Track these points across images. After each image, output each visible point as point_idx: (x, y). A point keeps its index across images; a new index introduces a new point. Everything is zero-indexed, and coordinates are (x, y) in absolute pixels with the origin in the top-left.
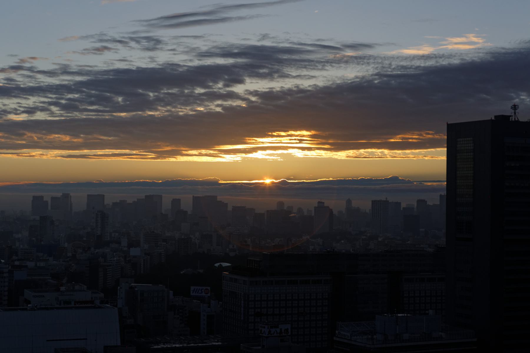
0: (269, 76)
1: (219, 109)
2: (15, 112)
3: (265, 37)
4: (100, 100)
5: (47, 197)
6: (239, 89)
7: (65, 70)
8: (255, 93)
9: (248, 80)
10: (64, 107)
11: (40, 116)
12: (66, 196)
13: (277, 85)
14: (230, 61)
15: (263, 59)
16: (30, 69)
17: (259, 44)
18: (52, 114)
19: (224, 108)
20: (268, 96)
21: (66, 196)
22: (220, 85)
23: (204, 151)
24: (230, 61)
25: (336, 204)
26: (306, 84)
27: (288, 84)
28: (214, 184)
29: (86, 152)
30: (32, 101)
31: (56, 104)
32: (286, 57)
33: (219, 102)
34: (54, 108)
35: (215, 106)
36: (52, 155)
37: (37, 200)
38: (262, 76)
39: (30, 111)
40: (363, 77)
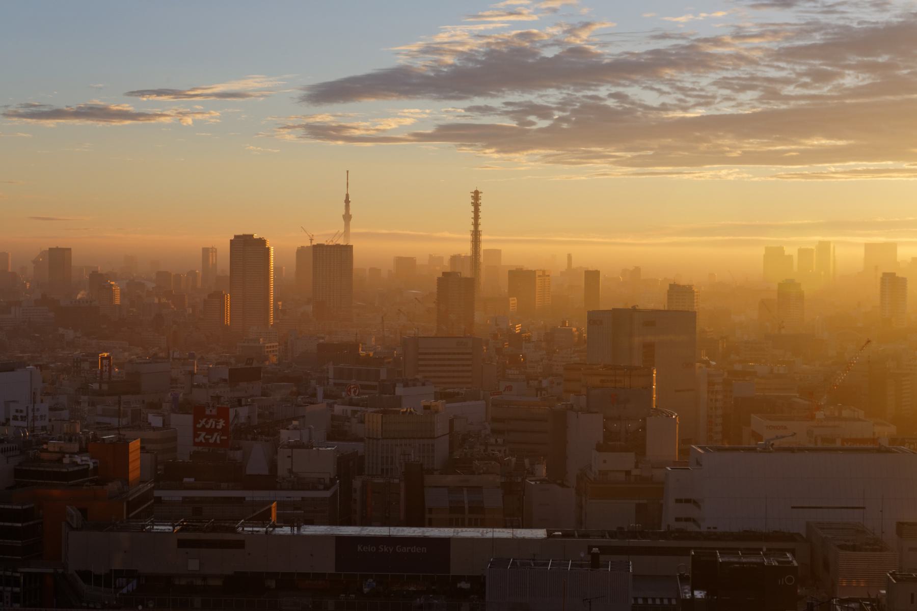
11: (726, 109)
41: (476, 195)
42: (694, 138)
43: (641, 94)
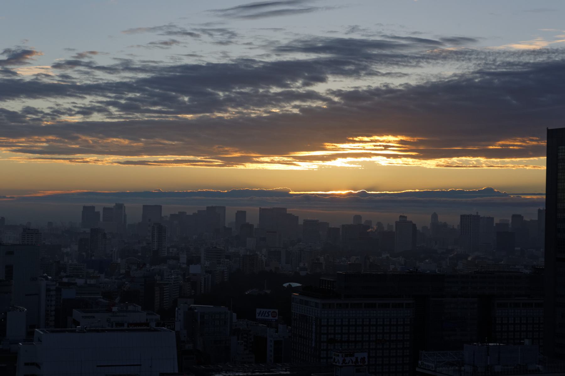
0: (355, 73)
1: (296, 111)
2: (69, 112)
3: (353, 29)
4: (164, 100)
5: (99, 207)
6: (320, 88)
7: (127, 66)
8: (339, 93)
9: (331, 78)
10: (123, 108)
11: (97, 117)
12: (120, 207)
13: (364, 83)
14: (312, 56)
15: (349, 54)
16: (88, 65)
17: (347, 37)
18: (110, 115)
19: (303, 110)
20: (353, 96)
21: (120, 207)
22: (299, 83)
23: (277, 158)
24: (312, 56)
25: (421, 219)
26: (396, 83)
27: (375, 82)
28: (283, 194)
29: (146, 157)
30: (88, 100)
31: (114, 104)
32: (375, 52)
33: (297, 103)
34: (112, 109)
35: (292, 108)
36: (109, 160)
37: (88, 211)
38: (347, 74)
39: (86, 111)
40: (463, 75)
41: (97, 366)
42: (67, 137)
43: (42, 104)
